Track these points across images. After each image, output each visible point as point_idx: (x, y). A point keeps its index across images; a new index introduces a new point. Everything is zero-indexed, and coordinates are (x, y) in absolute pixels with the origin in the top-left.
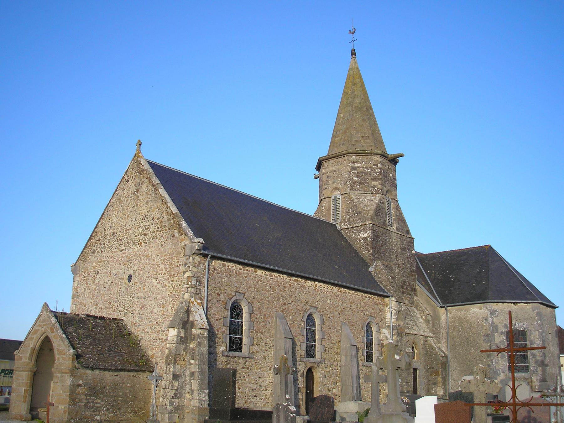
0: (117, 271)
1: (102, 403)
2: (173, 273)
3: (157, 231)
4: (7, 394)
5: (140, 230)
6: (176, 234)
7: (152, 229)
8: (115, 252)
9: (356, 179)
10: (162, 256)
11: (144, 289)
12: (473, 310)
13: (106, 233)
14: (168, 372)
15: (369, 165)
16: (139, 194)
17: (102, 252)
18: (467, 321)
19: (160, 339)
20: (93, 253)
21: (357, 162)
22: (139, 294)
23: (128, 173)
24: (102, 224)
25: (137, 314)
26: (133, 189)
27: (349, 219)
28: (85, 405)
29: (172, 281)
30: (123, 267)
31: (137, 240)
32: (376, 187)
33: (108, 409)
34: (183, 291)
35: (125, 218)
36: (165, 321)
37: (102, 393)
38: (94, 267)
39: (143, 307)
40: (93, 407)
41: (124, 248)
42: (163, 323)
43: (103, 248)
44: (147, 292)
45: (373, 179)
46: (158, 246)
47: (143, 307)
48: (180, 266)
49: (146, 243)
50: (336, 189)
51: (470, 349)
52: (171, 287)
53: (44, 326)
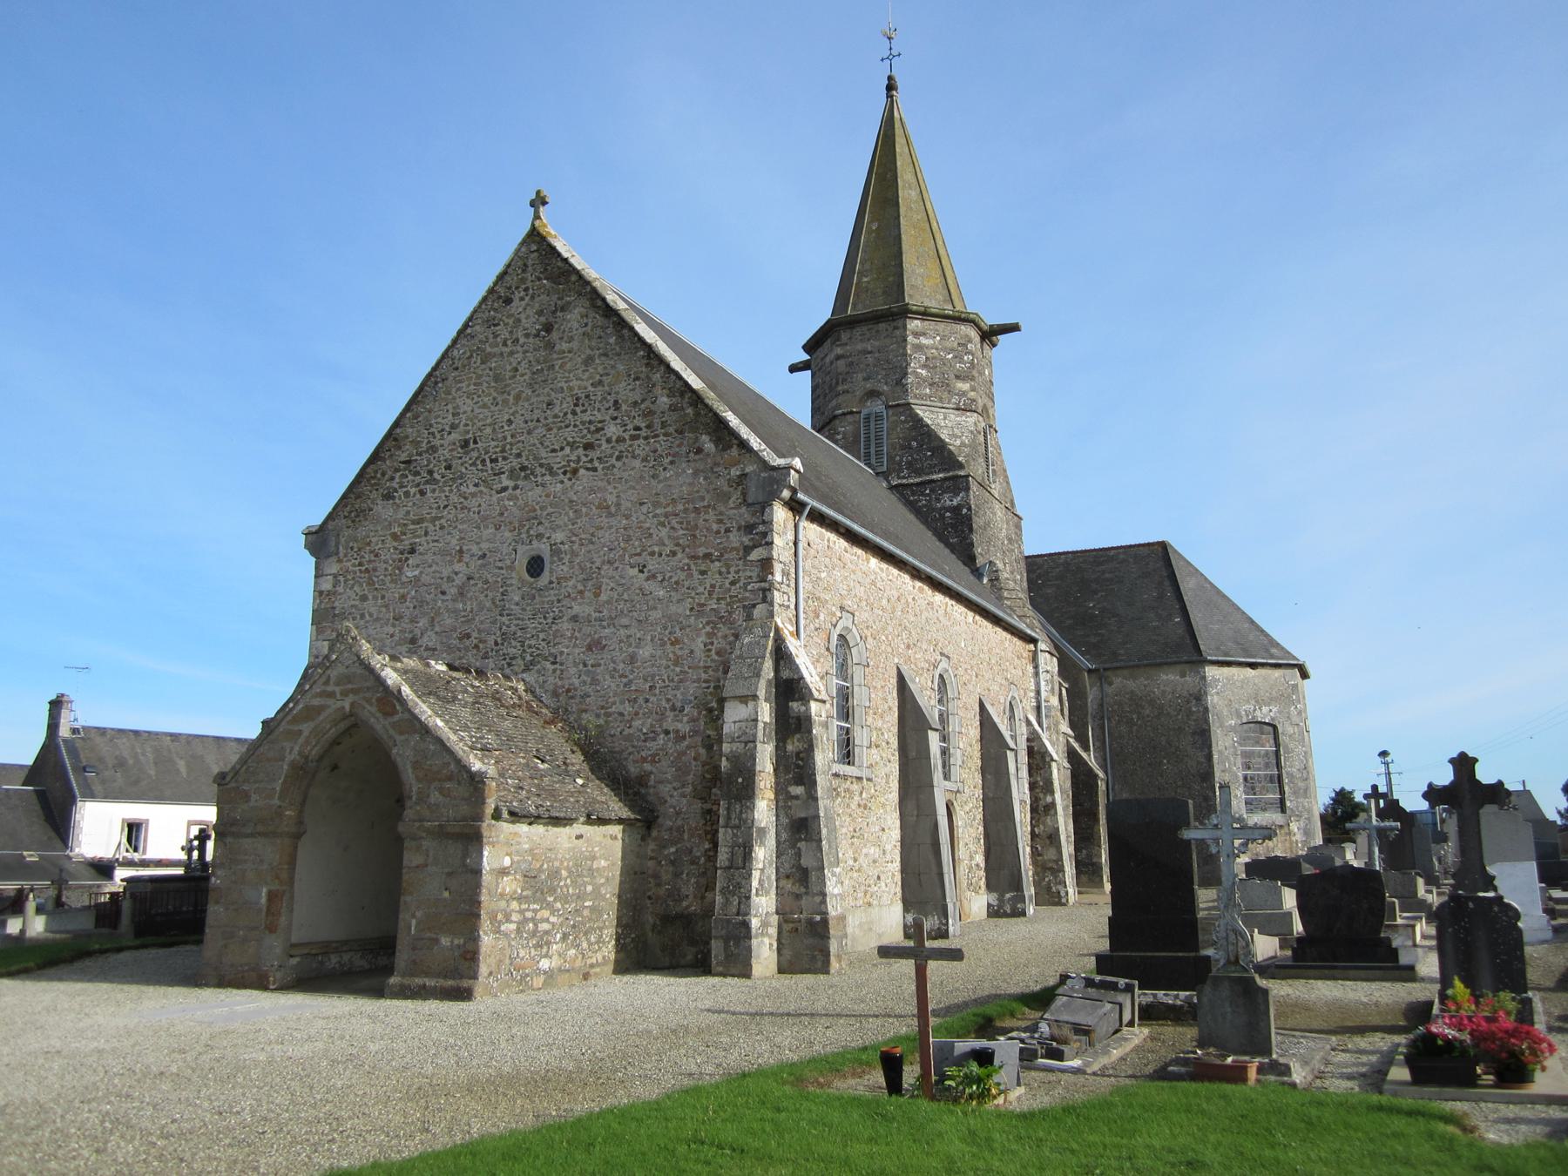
0: (485, 546)
1: (552, 919)
2: (701, 551)
3: (633, 438)
4: (764, 952)
5: (569, 434)
6: (709, 446)
7: (612, 430)
8: (474, 495)
9: (924, 372)
10: (656, 504)
11: (597, 595)
12: (1164, 677)
13: (437, 442)
14: (735, 822)
15: (948, 344)
16: (555, 335)
17: (422, 493)
18: (1152, 702)
19: (667, 732)
20: (388, 497)
21: (924, 334)
22: (577, 609)
23: (507, 278)
24: (416, 417)
25: (576, 664)
26: (530, 322)
27: (910, 464)
28: (518, 930)
29: (703, 573)
30: (507, 534)
31: (557, 461)
32: (964, 394)
33: (565, 937)
34: (745, 599)
35: (505, 402)
36: (681, 681)
37: (552, 890)
38: (395, 537)
39: (595, 645)
40: (534, 933)
41: (506, 482)
42: (677, 688)
43: (427, 482)
44: (608, 602)
45: (957, 377)
46: (642, 478)
47: (595, 645)
48: (728, 531)
49: (595, 470)
50: (873, 394)
51: (1161, 763)
52: (701, 589)
53: (345, 694)
